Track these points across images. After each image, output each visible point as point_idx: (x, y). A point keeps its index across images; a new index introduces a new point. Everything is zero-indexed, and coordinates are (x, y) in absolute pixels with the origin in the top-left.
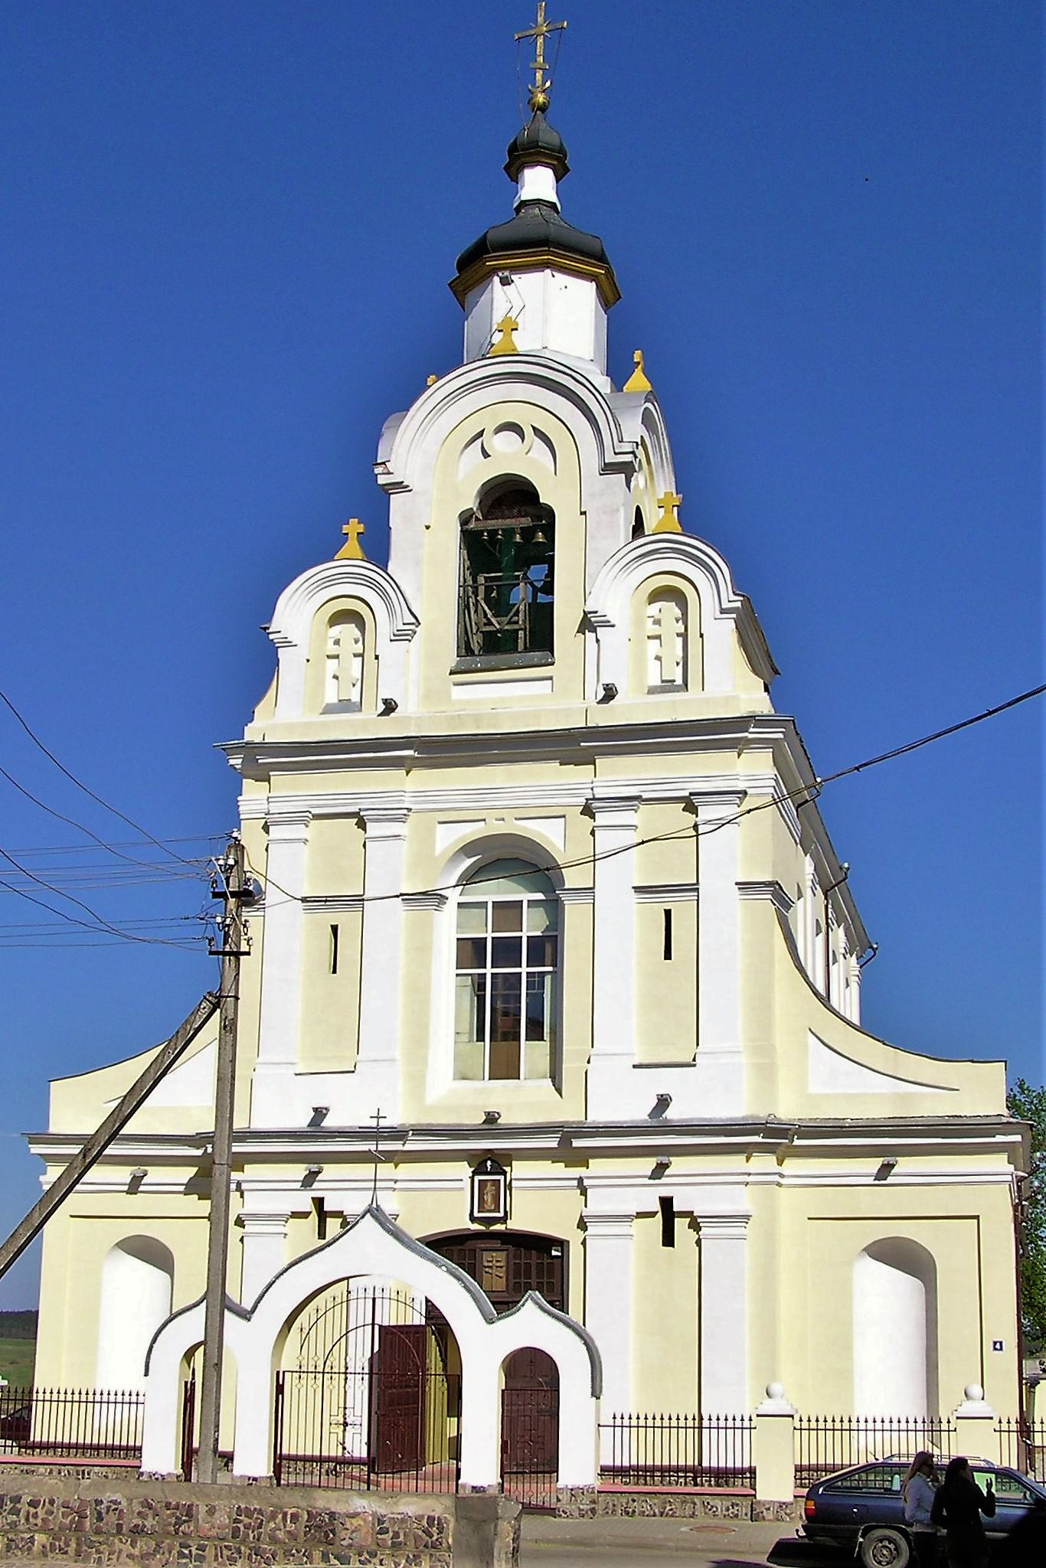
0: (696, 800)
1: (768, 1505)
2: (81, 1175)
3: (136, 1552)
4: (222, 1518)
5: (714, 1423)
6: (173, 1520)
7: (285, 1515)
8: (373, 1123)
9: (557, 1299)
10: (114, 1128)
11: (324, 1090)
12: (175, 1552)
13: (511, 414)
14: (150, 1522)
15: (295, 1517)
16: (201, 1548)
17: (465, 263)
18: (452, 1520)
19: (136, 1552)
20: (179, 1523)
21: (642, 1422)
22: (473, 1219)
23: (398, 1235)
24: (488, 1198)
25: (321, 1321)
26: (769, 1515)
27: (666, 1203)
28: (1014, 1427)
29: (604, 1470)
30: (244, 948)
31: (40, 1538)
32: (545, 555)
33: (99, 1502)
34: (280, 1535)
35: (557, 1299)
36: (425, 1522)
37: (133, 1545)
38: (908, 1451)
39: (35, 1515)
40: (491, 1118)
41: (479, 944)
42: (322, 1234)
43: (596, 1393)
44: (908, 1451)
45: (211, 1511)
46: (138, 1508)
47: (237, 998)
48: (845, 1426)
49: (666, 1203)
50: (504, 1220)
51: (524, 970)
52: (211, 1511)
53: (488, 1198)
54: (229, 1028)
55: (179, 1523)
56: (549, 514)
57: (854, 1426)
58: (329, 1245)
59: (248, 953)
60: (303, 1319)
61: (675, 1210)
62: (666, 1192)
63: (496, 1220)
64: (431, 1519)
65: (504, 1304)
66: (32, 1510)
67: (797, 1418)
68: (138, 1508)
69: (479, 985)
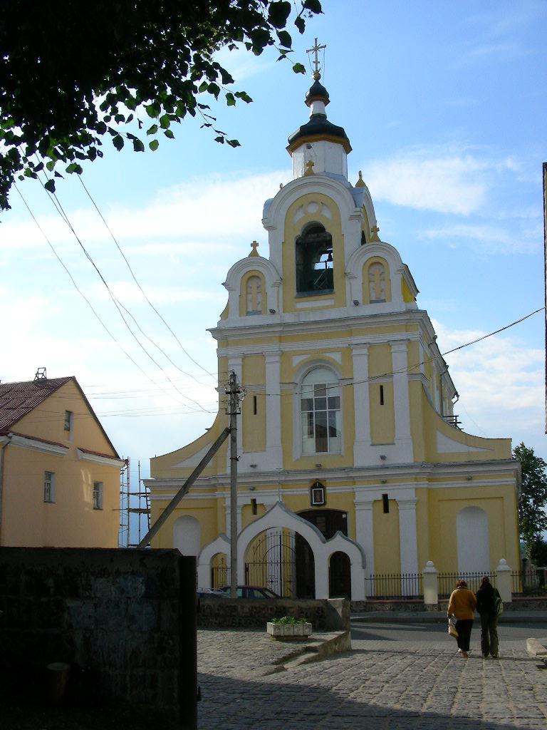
0: (390, 343)
1: (429, 605)
3: (217, 622)
4: (246, 610)
5: (405, 577)
14: (221, 612)
15: (271, 609)
19: (217, 622)
21: (384, 577)
22: (312, 505)
24: (318, 497)
26: (429, 609)
27: (385, 497)
28: (518, 574)
29: (367, 597)
30: (238, 411)
34: (267, 615)
37: (216, 619)
41: (310, 401)
43: (364, 567)
45: (243, 607)
49: (385, 497)
50: (325, 504)
52: (243, 607)
53: (318, 497)
54: (234, 440)
62: (384, 492)
63: (322, 505)
65: (328, 535)
69: (311, 415)
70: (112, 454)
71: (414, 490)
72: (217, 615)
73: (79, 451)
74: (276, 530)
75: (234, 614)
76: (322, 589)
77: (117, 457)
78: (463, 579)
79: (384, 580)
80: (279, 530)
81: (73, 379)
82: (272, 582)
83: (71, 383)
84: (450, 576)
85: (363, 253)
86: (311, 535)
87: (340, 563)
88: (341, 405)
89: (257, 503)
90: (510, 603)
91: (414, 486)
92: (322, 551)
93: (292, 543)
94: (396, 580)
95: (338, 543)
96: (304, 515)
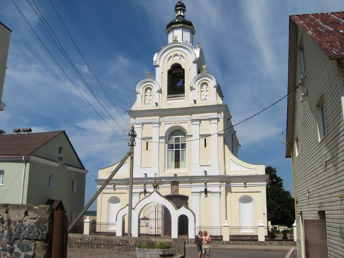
2: (106, 186)
6: (125, 243)
7: (144, 242)
8: (155, 176)
9: (187, 206)
10: (110, 178)
11: (146, 171)
12: (125, 248)
13: (176, 53)
14: (121, 243)
16: (130, 248)
17: (169, 26)
18: (173, 243)
20: (126, 243)
23: (161, 196)
25: (147, 211)
31: (102, 246)
32: (183, 77)
33: (112, 240)
35: (187, 206)
36: (168, 243)
38: (338, 228)
39: (101, 242)
40: (176, 175)
42: (145, 196)
44: (338, 228)
45: (131, 241)
46: (119, 241)
47: (133, 153)
48: (240, 228)
51: (180, 149)
54: (132, 158)
55: (126, 243)
56: (183, 70)
57: (241, 228)
58: (146, 198)
59: (135, 145)
60: (144, 210)
61: (207, 191)
64: (170, 243)
65: (178, 207)
66: (101, 241)
67: (230, 226)
68: (119, 241)
70: (82, 168)
71: (219, 187)
72: (119, 245)
73: (66, 166)
74: (155, 203)
75: (127, 244)
76: (175, 234)
77: (84, 168)
78: (283, 229)
79: (111, 225)
80: (156, 204)
81: (64, 132)
82: (151, 228)
83: (63, 135)
84: (237, 228)
85: (196, 81)
86: (170, 206)
87: (183, 221)
88: (187, 147)
89: (147, 191)
90: (264, 242)
91: (220, 185)
92: (175, 214)
93: (160, 209)
94: (218, 229)
95: (183, 211)
96: (168, 198)
